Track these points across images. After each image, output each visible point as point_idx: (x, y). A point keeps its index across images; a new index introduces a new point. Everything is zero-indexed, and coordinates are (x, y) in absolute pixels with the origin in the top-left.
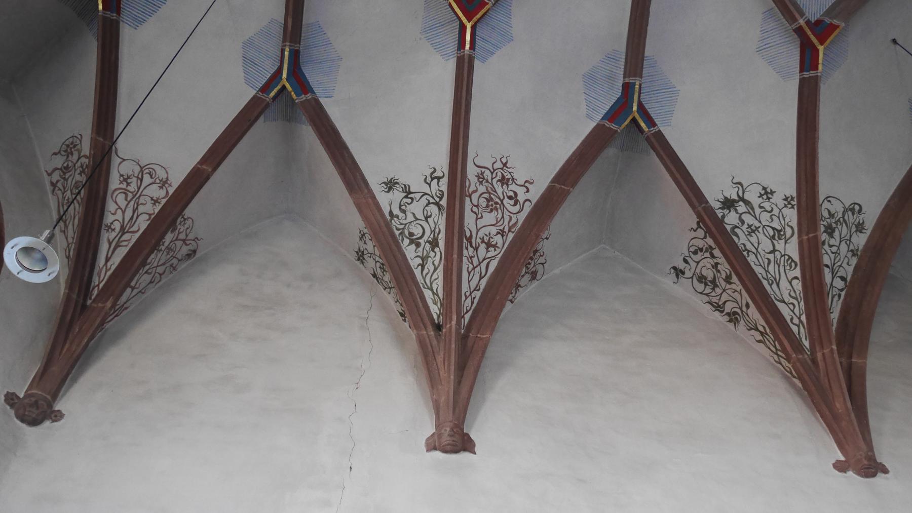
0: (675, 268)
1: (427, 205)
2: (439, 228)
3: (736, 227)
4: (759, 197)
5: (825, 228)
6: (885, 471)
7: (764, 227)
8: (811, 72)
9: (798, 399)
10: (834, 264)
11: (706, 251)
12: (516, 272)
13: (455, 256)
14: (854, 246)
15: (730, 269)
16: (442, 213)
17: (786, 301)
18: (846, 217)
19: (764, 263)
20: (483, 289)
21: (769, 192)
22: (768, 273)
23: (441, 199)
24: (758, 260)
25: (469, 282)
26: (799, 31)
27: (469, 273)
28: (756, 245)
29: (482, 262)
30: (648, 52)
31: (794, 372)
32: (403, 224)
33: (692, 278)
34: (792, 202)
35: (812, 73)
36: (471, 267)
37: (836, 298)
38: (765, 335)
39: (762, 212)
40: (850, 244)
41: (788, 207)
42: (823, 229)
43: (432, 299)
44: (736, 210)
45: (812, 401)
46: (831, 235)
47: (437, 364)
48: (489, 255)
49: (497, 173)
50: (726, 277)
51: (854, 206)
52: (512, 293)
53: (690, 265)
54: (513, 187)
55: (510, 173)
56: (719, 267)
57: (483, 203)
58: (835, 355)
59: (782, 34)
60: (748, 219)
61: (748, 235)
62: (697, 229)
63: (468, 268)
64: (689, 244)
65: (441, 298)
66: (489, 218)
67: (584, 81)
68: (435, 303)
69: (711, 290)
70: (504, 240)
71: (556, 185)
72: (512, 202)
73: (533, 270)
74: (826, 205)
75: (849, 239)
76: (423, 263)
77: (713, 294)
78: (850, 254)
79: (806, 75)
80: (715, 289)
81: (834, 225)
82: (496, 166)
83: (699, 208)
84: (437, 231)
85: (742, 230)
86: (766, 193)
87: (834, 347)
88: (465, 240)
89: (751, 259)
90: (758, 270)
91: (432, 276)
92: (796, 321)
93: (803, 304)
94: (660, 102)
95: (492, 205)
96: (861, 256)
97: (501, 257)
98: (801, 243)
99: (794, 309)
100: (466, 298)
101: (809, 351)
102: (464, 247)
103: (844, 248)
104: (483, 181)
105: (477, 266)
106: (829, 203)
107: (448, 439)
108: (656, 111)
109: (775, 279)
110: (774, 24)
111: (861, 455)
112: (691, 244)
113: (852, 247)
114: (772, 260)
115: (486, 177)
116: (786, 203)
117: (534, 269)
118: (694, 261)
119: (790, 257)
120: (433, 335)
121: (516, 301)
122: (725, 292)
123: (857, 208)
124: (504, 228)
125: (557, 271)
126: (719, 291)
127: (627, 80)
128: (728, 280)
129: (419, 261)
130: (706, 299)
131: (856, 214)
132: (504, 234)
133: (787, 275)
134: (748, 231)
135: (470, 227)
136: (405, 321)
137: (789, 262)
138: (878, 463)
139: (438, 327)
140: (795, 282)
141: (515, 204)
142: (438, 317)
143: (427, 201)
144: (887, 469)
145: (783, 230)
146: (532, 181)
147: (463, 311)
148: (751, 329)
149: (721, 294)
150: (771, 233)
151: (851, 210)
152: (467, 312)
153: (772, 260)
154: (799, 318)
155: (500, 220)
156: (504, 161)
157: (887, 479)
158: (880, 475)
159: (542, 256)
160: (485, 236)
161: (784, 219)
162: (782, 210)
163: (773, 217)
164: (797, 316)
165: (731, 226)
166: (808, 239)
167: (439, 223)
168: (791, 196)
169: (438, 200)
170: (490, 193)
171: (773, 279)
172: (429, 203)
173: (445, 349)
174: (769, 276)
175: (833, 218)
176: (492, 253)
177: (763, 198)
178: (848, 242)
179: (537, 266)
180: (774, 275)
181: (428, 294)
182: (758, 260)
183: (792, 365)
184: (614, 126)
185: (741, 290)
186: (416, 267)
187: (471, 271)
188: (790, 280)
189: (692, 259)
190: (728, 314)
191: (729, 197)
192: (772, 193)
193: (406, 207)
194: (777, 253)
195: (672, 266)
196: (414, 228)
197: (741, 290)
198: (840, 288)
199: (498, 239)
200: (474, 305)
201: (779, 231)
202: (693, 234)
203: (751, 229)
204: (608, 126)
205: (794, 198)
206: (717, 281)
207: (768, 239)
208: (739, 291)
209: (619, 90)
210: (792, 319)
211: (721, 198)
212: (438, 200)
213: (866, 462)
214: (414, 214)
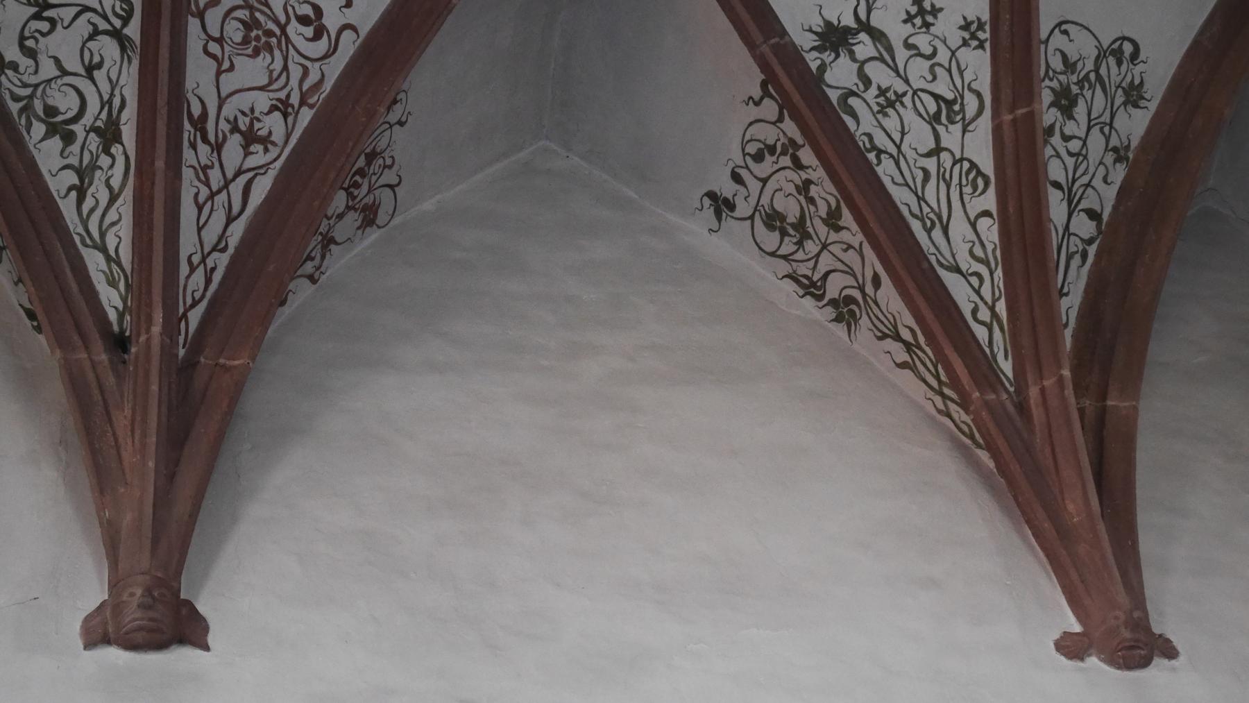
0: (711, 195)
1: (91, 37)
2: (122, 95)
3: (853, 94)
4: (905, 22)
5: (1055, 95)
6: (1170, 652)
7: (915, 93)
9: (985, 497)
10: (1074, 181)
11: (784, 153)
12: (316, 203)
13: (160, 164)
14: (1120, 139)
15: (836, 193)
16: (129, 57)
17: (964, 267)
18: (1103, 71)
19: (914, 179)
20: (236, 248)
21: (929, 9)
22: (922, 203)
23: (126, 21)
25: (200, 230)
27: (200, 209)
28: (897, 137)
29: (234, 179)
31: (977, 435)
32: (29, 86)
33: (752, 218)
34: (981, 35)
36: (204, 192)
37: (1077, 260)
38: (916, 350)
39: (911, 57)
40: (1110, 132)
41: (969, 46)
42: (1047, 97)
43: (104, 272)
44: (852, 54)
45: (1016, 498)
46: (1068, 112)
47: (114, 434)
48: (252, 162)
50: (828, 214)
51: (1122, 44)
52: (312, 259)
53: (746, 187)
56: (814, 191)
57: (235, 32)
58: (1066, 392)
60: (880, 75)
61: (879, 112)
62: (762, 99)
63: (197, 195)
64: (744, 135)
65: (129, 272)
66: (251, 70)
68: (112, 283)
69: (796, 247)
70: (290, 126)
72: (309, 31)
73: (366, 200)
74: (1058, 40)
75: (1108, 121)
76: (82, 180)
77: (800, 255)
78: (1109, 158)
80: (805, 243)
81: (1075, 89)
83: (764, 46)
84: (117, 102)
85: (865, 101)
86: (922, 12)
87: (1066, 373)
88: (187, 125)
89: (886, 170)
90: (901, 195)
91: (104, 215)
92: (984, 315)
93: (1001, 275)
95: (258, 38)
96: (1135, 159)
97: (282, 169)
98: (997, 130)
99: (980, 286)
100: (193, 269)
101: (1011, 385)
102: (186, 144)
103: (1096, 142)
105: (219, 191)
106: (1065, 36)
107: (138, 614)
109: (940, 218)
111: (1116, 618)
112: (747, 137)
113: (1114, 141)
114: (933, 170)
116: (967, 36)
117: (369, 200)
118: (755, 177)
119: (973, 165)
120: (106, 363)
121: (323, 277)
122: (825, 251)
123: (1128, 48)
124: (288, 96)
125: (428, 205)
126: (811, 247)
128: (832, 219)
129: (71, 178)
130: (785, 268)
131: (1125, 62)
133: (968, 206)
134: (878, 104)
135: (200, 92)
136: (38, 329)
137: (971, 176)
138: (1154, 634)
139: (119, 343)
140: (984, 223)
141: (317, 36)
142: (121, 316)
143: (91, 28)
144: (1174, 648)
145: (959, 101)
147: (185, 303)
148: (884, 336)
149: (818, 255)
150: (932, 107)
151: (1113, 53)
152: (193, 306)
153: (933, 170)
154: (992, 309)
155: (280, 76)
157: (1174, 669)
158: (1159, 662)
159: (390, 167)
161: (961, 73)
162: (956, 54)
163: (937, 69)
164: (986, 303)
165: (840, 92)
166: (1014, 121)
167: (122, 82)
168: (979, 19)
169: (118, 23)
170: (251, 8)
171: (935, 218)
172: (95, 33)
173: (135, 397)
174: (926, 209)
175: (1073, 73)
176: (258, 158)
177: (914, 25)
178: (1107, 129)
179: (377, 192)
180: (935, 206)
181: (94, 262)
183: (972, 417)
185: (861, 244)
186: (63, 193)
187: (205, 203)
188: (972, 219)
189: (751, 173)
190: (834, 303)
191: (836, 23)
192: (935, 11)
193: (37, 41)
194: (945, 156)
196: (57, 94)
197: (861, 244)
198: (1086, 237)
199: (274, 124)
200: (214, 286)
201: (950, 103)
202: (754, 112)
205: (986, 23)
206: (808, 223)
207: (925, 123)
208: (857, 248)
210: (975, 312)
211: (817, 23)
212: (118, 23)
213: (1127, 634)
214: (57, 61)
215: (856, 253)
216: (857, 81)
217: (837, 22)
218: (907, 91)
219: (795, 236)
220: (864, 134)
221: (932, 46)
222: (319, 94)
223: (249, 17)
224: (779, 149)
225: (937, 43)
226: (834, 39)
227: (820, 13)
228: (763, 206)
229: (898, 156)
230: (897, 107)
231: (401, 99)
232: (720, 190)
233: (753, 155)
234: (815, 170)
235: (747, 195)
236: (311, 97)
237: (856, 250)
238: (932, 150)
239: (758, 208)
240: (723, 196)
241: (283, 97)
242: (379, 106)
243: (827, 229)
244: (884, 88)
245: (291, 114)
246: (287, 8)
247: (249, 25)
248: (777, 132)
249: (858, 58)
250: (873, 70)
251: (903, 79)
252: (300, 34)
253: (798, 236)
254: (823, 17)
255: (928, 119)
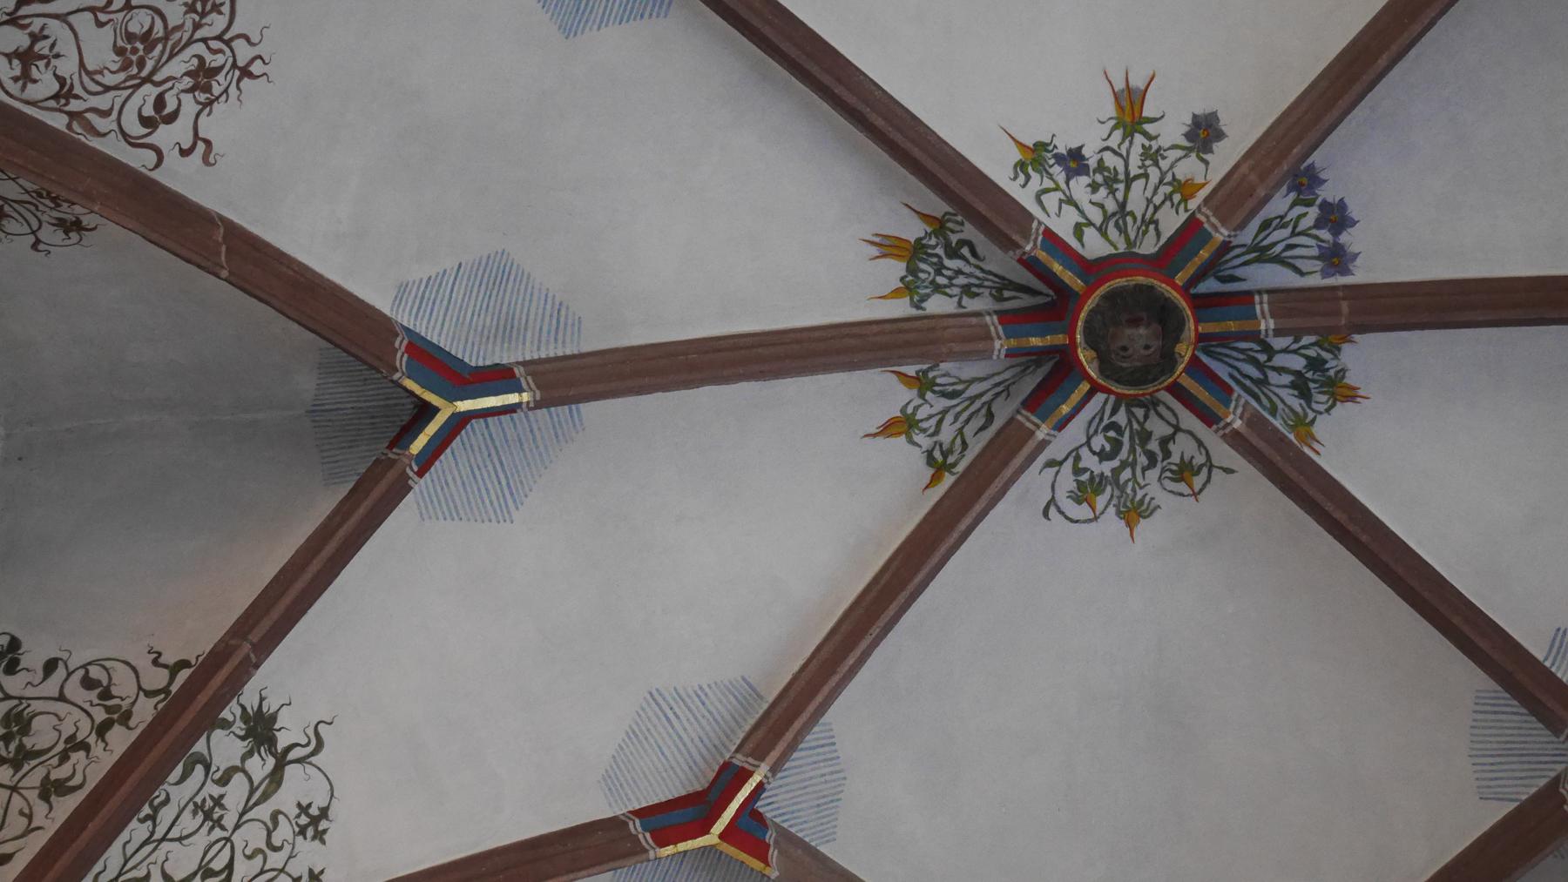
0: (15, 644)
3: (207, 767)
4: (299, 805)
7: (228, 840)
8: (648, 835)
11: (108, 709)
19: (134, 867)
21: (320, 828)
24: (137, 851)
26: (730, 777)
28: (174, 833)
30: (590, 410)
35: (646, 839)
44: (249, 754)
49: (220, 51)
50: (56, 780)
54: (189, 106)
55: (226, 91)
56: (78, 756)
59: (705, 739)
60: (235, 794)
61: (195, 804)
62: (165, 666)
66: (100, 47)
67: (489, 257)
71: (222, 230)
72: (149, 111)
79: (636, 826)
82: (241, 48)
86: (315, 821)
89: (136, 831)
94: (475, 477)
95: (135, 50)
104: (196, 12)
108: (451, 472)
110: (725, 713)
112: (108, 664)
115: (207, 20)
122: (9, 792)
124: (77, 97)
127: (519, 371)
132: (63, 101)
134: (204, 800)
141: (146, 121)
146: (211, 160)
150: (217, 865)
155: (98, 83)
156: (256, 68)
160: (50, 41)
163: (260, 857)
165: (205, 752)
177: (298, 816)
182: (137, 851)
184: (402, 360)
189: (66, 680)
191: (277, 726)
192: (320, 836)
195: (18, 634)
199: (45, 85)
202: (144, 663)
203: (213, 808)
204: (397, 344)
206: (34, 763)
207: (199, 861)
208: (33, 826)
209: (484, 359)
211: (270, 706)
215: (25, 826)
216: (222, 769)
217: (278, 728)
218: (226, 830)
219: (10, 752)
220: (168, 795)
221: (283, 844)
222: (85, 133)
223: (157, 36)
224: (109, 703)
225: (287, 849)
226: (259, 730)
227: (283, 705)
228: (29, 706)
229: (154, 841)
230: (206, 823)
231: (70, 238)
232: (26, 651)
233: (88, 677)
234: (105, 750)
235: (36, 683)
236: (79, 124)
237: (29, 824)
238: (172, 878)
239: (24, 701)
240: (20, 656)
241: (75, 92)
242: (101, 204)
243: (38, 784)
244: (222, 802)
245: (58, 104)
246: (171, 80)
247: (147, 40)
248: (131, 695)
249: (247, 762)
250: (238, 785)
251: (238, 821)
252: (145, 101)
253: (11, 755)
254: (278, 710)
255: (203, 864)
